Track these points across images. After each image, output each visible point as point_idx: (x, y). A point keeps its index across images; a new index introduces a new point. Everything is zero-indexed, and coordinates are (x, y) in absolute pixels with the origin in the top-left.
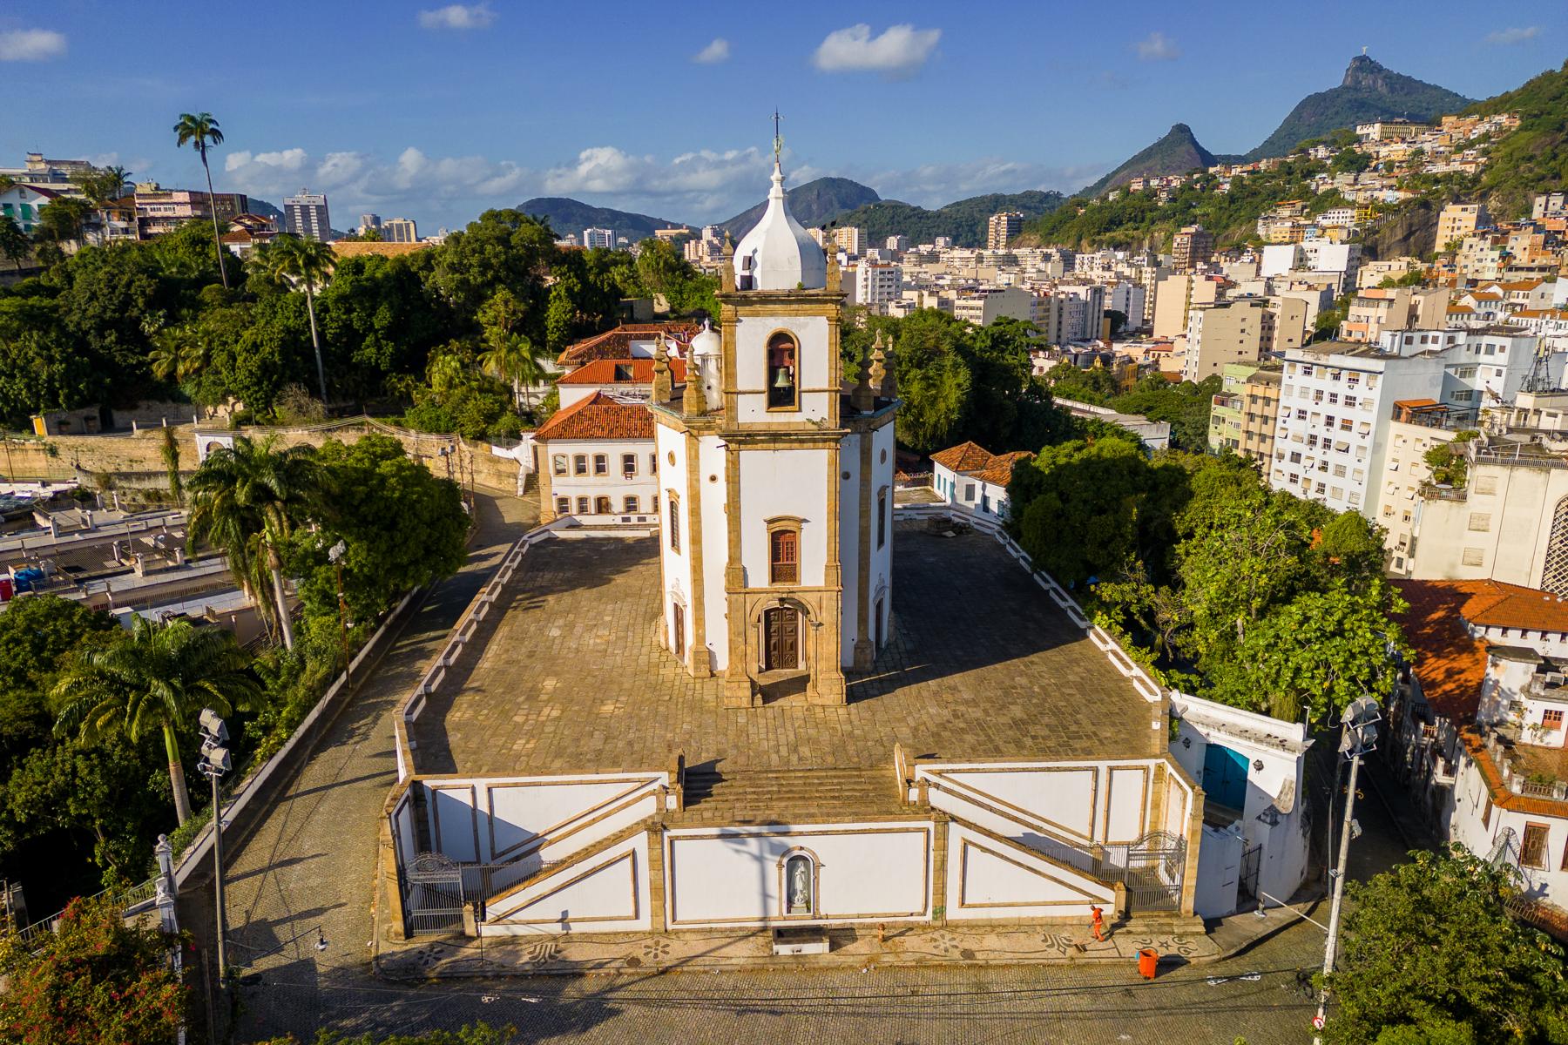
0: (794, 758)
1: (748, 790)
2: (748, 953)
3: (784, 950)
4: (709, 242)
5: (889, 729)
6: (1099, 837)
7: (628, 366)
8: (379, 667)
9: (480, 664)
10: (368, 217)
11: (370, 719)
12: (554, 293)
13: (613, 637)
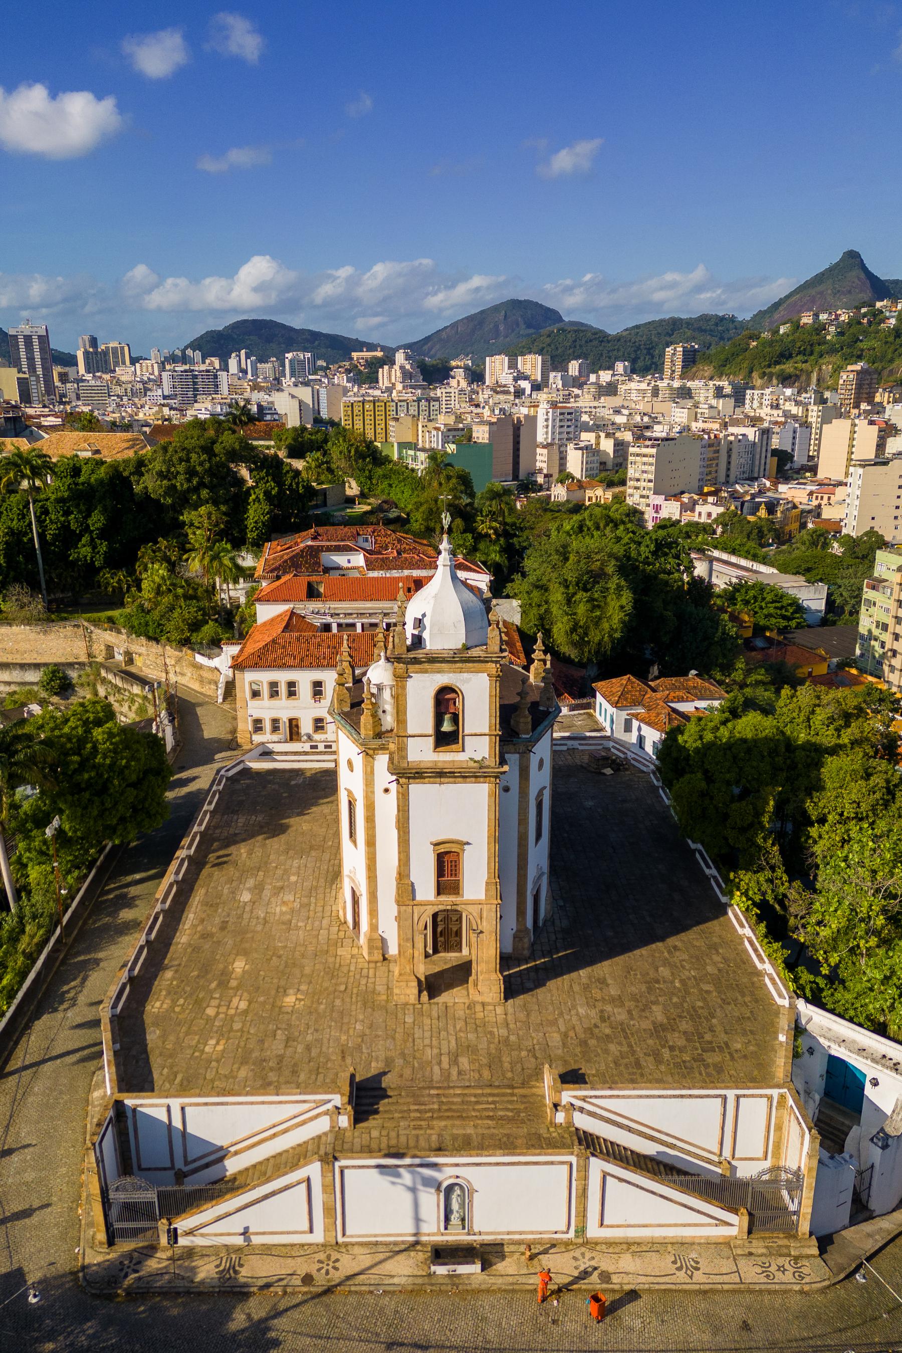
0: (454, 1072)
1: (413, 1107)
2: (408, 1271)
3: (441, 1270)
4: (402, 368)
5: (541, 1034)
6: (727, 1153)
7: (318, 583)
8: (89, 917)
10: (86, 338)
11: (79, 980)
12: (253, 497)
13: (297, 905)
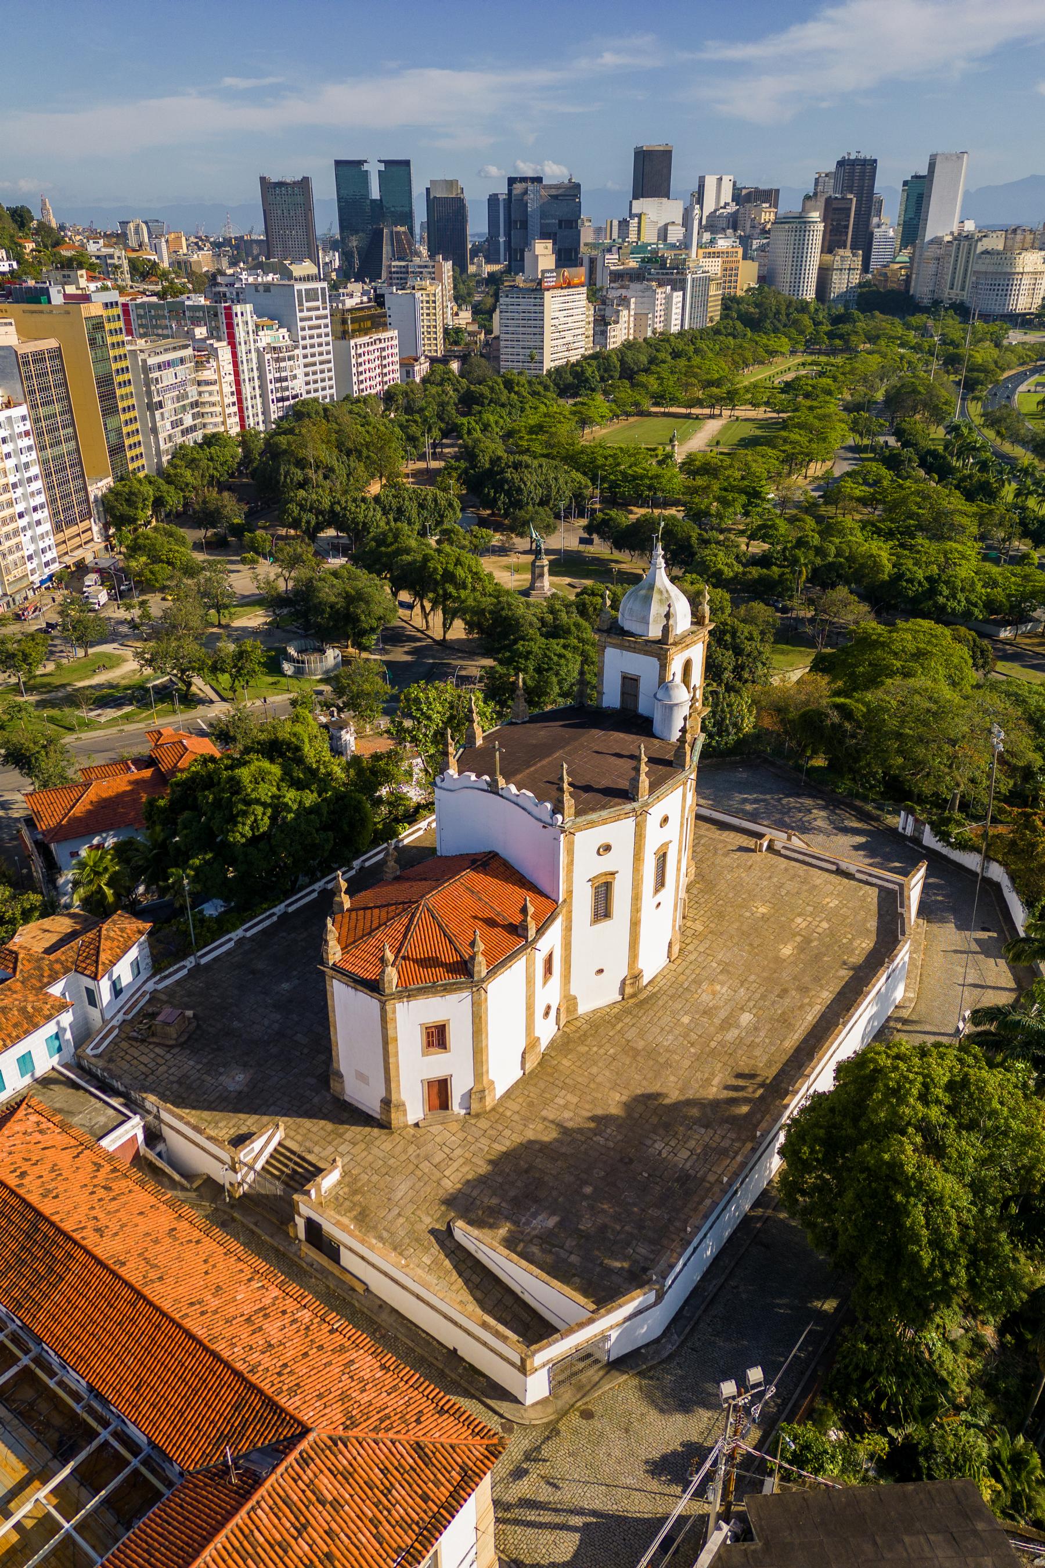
9: (831, 996)
